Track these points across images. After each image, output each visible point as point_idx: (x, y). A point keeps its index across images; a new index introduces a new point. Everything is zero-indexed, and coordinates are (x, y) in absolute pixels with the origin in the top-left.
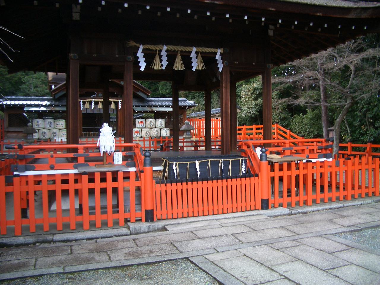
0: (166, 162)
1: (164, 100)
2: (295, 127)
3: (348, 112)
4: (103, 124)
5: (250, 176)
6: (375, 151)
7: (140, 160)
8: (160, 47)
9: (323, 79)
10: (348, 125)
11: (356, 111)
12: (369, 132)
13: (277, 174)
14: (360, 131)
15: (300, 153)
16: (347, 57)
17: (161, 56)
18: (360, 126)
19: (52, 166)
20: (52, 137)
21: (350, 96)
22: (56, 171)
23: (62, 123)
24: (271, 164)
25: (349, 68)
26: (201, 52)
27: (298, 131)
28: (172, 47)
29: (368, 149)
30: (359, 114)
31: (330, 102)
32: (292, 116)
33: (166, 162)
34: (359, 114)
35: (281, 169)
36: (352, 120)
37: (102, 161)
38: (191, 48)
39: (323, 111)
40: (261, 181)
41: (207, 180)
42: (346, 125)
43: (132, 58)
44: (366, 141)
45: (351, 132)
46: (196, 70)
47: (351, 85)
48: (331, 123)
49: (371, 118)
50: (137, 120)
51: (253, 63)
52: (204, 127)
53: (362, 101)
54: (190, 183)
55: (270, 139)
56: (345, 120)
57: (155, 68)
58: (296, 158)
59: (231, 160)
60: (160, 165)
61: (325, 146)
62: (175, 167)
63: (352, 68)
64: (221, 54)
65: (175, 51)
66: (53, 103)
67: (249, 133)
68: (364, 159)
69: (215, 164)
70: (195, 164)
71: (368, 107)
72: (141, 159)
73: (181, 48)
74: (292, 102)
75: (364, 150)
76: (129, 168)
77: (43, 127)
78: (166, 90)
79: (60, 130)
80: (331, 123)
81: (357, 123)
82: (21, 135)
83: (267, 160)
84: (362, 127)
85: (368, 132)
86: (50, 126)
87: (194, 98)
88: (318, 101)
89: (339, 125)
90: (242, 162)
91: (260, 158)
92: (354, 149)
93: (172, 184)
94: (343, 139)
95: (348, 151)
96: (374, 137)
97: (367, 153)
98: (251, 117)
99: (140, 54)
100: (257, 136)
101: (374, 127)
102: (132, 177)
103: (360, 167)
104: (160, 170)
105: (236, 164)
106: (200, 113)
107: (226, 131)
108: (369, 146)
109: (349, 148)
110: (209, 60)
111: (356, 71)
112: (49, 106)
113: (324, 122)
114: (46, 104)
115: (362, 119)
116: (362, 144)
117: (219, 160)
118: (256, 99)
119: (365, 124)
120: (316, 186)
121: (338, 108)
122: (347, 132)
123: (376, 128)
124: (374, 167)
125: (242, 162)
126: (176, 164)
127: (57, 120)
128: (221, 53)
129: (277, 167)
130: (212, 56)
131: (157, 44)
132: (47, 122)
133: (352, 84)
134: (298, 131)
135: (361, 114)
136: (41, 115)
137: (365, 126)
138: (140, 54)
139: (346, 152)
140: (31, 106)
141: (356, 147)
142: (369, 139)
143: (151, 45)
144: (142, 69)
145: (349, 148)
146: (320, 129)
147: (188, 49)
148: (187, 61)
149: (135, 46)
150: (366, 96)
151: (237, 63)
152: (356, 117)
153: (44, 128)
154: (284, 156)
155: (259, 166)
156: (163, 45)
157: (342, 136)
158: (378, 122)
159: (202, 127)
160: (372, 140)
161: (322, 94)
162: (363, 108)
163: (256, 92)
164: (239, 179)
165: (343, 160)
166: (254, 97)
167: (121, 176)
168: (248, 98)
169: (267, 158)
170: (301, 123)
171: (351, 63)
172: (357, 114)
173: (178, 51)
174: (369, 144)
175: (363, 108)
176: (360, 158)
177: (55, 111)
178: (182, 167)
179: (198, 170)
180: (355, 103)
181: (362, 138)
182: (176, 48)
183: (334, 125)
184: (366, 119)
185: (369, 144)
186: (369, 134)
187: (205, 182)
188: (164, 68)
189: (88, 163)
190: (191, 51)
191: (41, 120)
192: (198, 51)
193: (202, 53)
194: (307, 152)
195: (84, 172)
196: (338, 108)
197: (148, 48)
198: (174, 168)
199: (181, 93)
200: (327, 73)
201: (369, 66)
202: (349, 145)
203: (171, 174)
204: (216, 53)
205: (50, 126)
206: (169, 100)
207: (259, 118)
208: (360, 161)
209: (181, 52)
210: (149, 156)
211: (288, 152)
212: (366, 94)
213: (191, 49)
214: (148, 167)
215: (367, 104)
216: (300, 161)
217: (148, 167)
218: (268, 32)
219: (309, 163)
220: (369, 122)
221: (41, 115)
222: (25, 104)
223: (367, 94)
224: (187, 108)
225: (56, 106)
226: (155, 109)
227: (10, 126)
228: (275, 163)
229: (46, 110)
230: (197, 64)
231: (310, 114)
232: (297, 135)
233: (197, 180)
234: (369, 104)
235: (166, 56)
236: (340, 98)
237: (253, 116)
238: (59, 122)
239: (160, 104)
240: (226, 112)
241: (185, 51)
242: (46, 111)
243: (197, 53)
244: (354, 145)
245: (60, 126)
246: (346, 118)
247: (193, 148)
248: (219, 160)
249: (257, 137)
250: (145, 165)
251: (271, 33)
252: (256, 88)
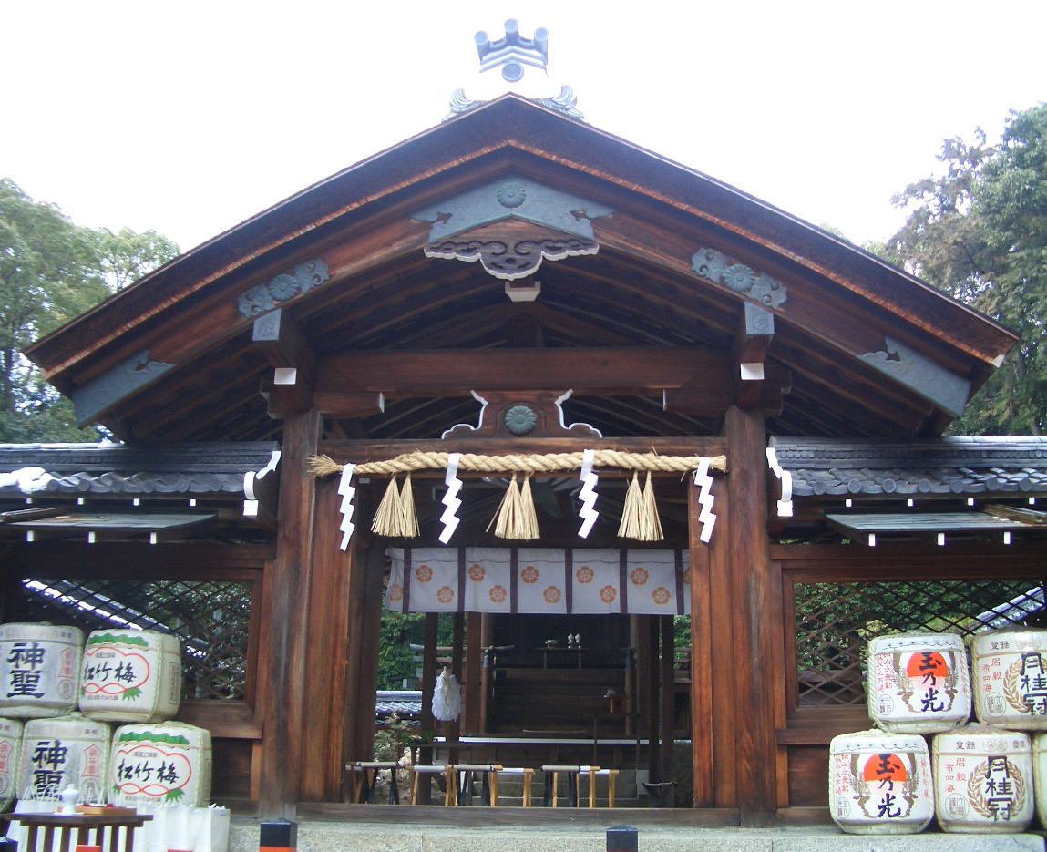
79: (115, 725)
245: (107, 694)
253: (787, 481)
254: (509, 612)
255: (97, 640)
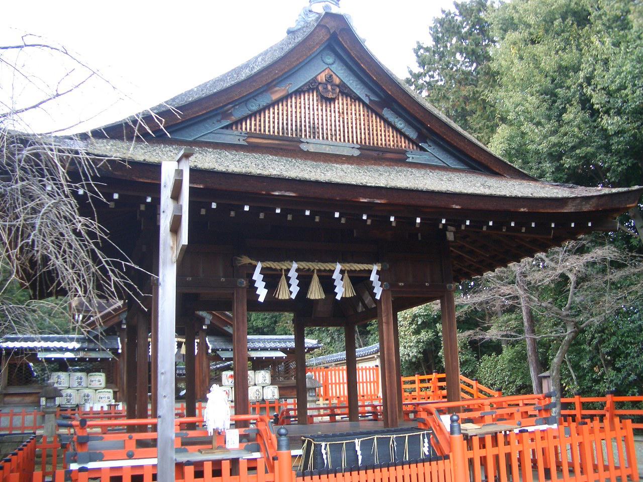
0: (309, 443)
1: (268, 340)
2: (485, 375)
3: (570, 344)
4: (210, 386)
5: (437, 459)
6: (621, 408)
7: (270, 441)
8: (287, 265)
9: (528, 297)
10: (572, 366)
11: (582, 344)
12: (607, 377)
13: (477, 453)
14: (592, 375)
15: (506, 420)
16: (562, 261)
17: (288, 279)
18: (591, 368)
19: (130, 453)
20: (82, 403)
21: (573, 321)
22: (137, 460)
23: (99, 378)
24: (468, 439)
25: (567, 278)
26: (348, 271)
27: (490, 382)
28: (304, 265)
29: (608, 405)
30: (588, 348)
31: (539, 332)
32: (478, 358)
33: (309, 443)
34: (588, 348)
35: (483, 445)
36: (577, 359)
37: (210, 442)
38: (333, 265)
39: (529, 348)
40: (454, 466)
41: (373, 467)
42: (569, 367)
43: (245, 283)
44: (604, 392)
45: (578, 377)
46: (342, 298)
47: (571, 304)
48: (544, 365)
49: (608, 354)
50: (224, 373)
51: (427, 284)
52: (345, 381)
53: (590, 328)
54: (347, 474)
55: (458, 400)
56: (566, 360)
57: (280, 297)
58: (501, 427)
59: (407, 435)
60: (299, 448)
61: (545, 406)
62: (325, 449)
63: (572, 278)
64: (378, 273)
65: (309, 269)
66: (86, 345)
67: (409, 389)
68: (606, 422)
69: (383, 442)
70: (354, 443)
71: (602, 336)
72: (270, 439)
73: (319, 265)
74: (481, 337)
75: (603, 406)
76: (253, 453)
77: (68, 386)
78: (263, 320)
79: (96, 390)
80: (544, 365)
81: (586, 364)
82: (28, 399)
83: (460, 433)
84: (595, 369)
85: (605, 377)
86: (80, 384)
87: (312, 333)
88: (521, 332)
89: (557, 369)
90: (424, 438)
91: (449, 430)
92: (585, 406)
93: (321, 476)
94: (565, 391)
95: (575, 409)
96: (616, 384)
97: (608, 411)
98: (410, 361)
99: (257, 276)
100: (423, 393)
101: (614, 369)
102: (261, 467)
103: (602, 435)
104: (300, 456)
105: (415, 442)
106: (323, 358)
107: (391, 390)
108: (609, 398)
109: (578, 406)
110: (360, 281)
111: (577, 283)
112: (79, 350)
113: (533, 365)
114: (74, 348)
115: (594, 357)
116: (598, 396)
117: (389, 436)
118: (417, 332)
119: (599, 363)
120: (537, 471)
121: (553, 341)
122: (572, 379)
123: (619, 370)
124: (626, 435)
125: (424, 438)
126: (326, 445)
127: (91, 374)
128: (378, 271)
129: (476, 442)
130: (365, 275)
131: (282, 261)
132: (75, 378)
133: (573, 302)
134: (490, 382)
135: (591, 348)
136: (62, 365)
137: (599, 367)
138: (257, 276)
139: (573, 412)
140: (48, 350)
141: (587, 402)
142: (608, 388)
143: (274, 262)
144: (261, 299)
145: (578, 406)
146: (526, 375)
147: (328, 266)
148: (328, 285)
149: (250, 264)
150: (596, 321)
151: (403, 284)
152: (583, 354)
153: (69, 388)
154: (484, 425)
155: (450, 443)
156: (291, 261)
157: (564, 385)
158: (619, 360)
159: (330, 382)
160: (614, 389)
161: (525, 320)
162: (593, 338)
163: (417, 322)
164: (420, 465)
165: (573, 425)
166: (415, 329)
167: (243, 467)
168: (405, 331)
169: (460, 429)
170: (494, 368)
171: (571, 270)
172: (584, 349)
173: (313, 271)
174: (609, 397)
175: (593, 338)
176: (601, 421)
177: (89, 358)
178: (336, 449)
179: (359, 453)
180: (580, 331)
181: (597, 388)
182: (311, 267)
183: (549, 368)
184: (600, 357)
185: (609, 397)
186: (607, 379)
187: (370, 472)
188: (293, 296)
189: (187, 447)
190: (333, 269)
191: (64, 373)
192: (343, 269)
193: (350, 272)
194: (518, 416)
195: (188, 461)
196: (553, 341)
197: (269, 266)
198: (323, 451)
199: (306, 330)
200: (531, 288)
201: (597, 273)
202: (576, 400)
203: (319, 461)
204: (370, 271)
205: (80, 385)
206: (276, 339)
207: (428, 361)
208: (602, 425)
209: (319, 271)
210: (285, 435)
211: (488, 419)
212: (597, 317)
213: (333, 267)
214: (284, 451)
215: (599, 332)
216: (510, 431)
217: (284, 451)
218: (445, 235)
219: (525, 434)
220: (605, 360)
221: (62, 365)
222: (39, 348)
223: (598, 318)
224: (306, 351)
225: (90, 350)
226: (254, 355)
227: (11, 385)
228: (471, 437)
229: (74, 357)
230: (344, 289)
231: (507, 352)
232: (489, 388)
233: (358, 469)
234: (603, 331)
235: (297, 278)
236: (555, 325)
237: (414, 360)
238: (95, 377)
239: (261, 345)
240: (390, 361)
241: (325, 270)
242: (74, 359)
243: (342, 272)
244: (584, 399)
245: (96, 384)
246: (567, 356)
247: (327, 418)
248: (389, 436)
249: (423, 396)
250: (279, 447)
251: (450, 236)
252: (417, 315)
253: (210, 346)
254: (249, 398)
255: (90, 376)
